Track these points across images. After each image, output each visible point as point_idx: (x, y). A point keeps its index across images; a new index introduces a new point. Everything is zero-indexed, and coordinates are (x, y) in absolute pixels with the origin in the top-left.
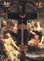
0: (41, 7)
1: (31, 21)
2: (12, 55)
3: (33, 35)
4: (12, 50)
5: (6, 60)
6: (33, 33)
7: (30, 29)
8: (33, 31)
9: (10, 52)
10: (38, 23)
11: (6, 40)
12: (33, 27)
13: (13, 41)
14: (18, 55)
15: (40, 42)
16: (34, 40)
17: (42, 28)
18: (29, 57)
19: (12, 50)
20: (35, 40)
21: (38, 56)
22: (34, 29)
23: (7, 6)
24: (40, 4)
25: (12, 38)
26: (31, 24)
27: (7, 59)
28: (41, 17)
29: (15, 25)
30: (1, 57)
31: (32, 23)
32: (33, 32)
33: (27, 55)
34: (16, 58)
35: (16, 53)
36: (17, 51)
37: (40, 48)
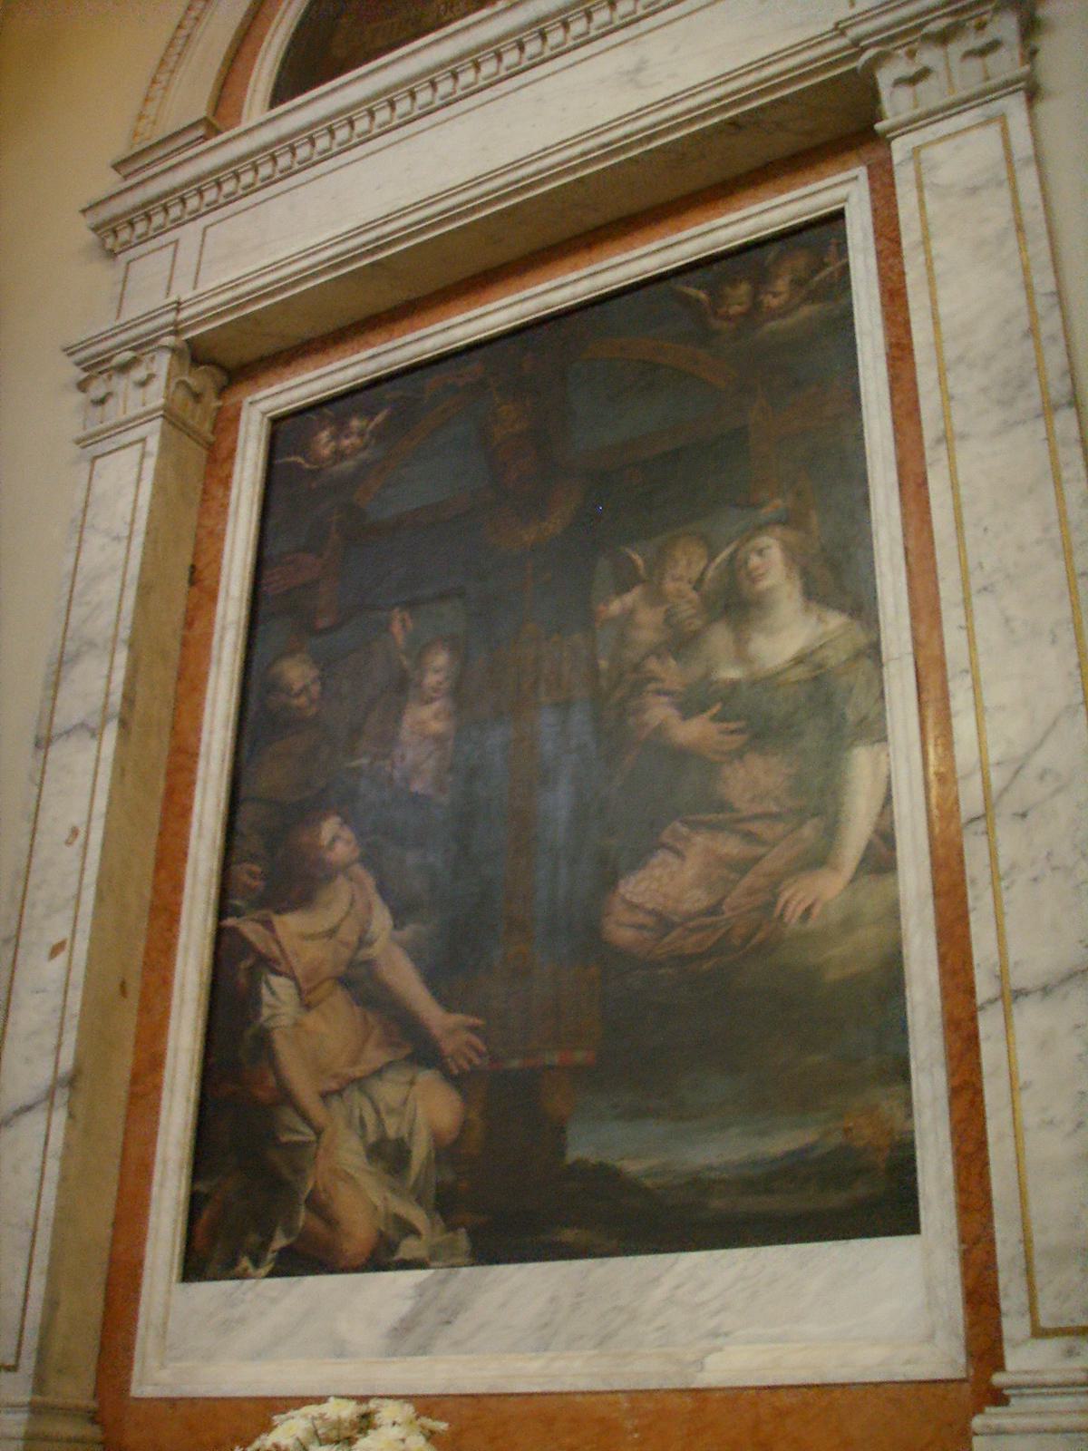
0: (807, 311)
1: (659, 561)
2: (348, 1153)
3: (682, 756)
4: (359, 1083)
5: (264, 1246)
6: (691, 731)
7: (638, 688)
8: (690, 706)
9: (334, 1118)
10: (775, 554)
11: (291, 924)
12: (681, 642)
13: (381, 920)
14: (445, 1152)
15: (819, 859)
16: (701, 840)
17: (835, 621)
18: (632, 1167)
19: (357, 1072)
20: (731, 846)
21: (782, 1142)
22: (697, 670)
23: (348, 465)
24: (782, 285)
25: (370, 882)
26: (656, 596)
27: (280, 1242)
28: (356, 732)
29: (431, 679)
30: (300, 460)
31: (670, 586)
32: (685, 718)
33: (583, 1146)
34: (417, 1216)
35: (421, 1120)
36: (427, 1077)
37: (833, 975)
